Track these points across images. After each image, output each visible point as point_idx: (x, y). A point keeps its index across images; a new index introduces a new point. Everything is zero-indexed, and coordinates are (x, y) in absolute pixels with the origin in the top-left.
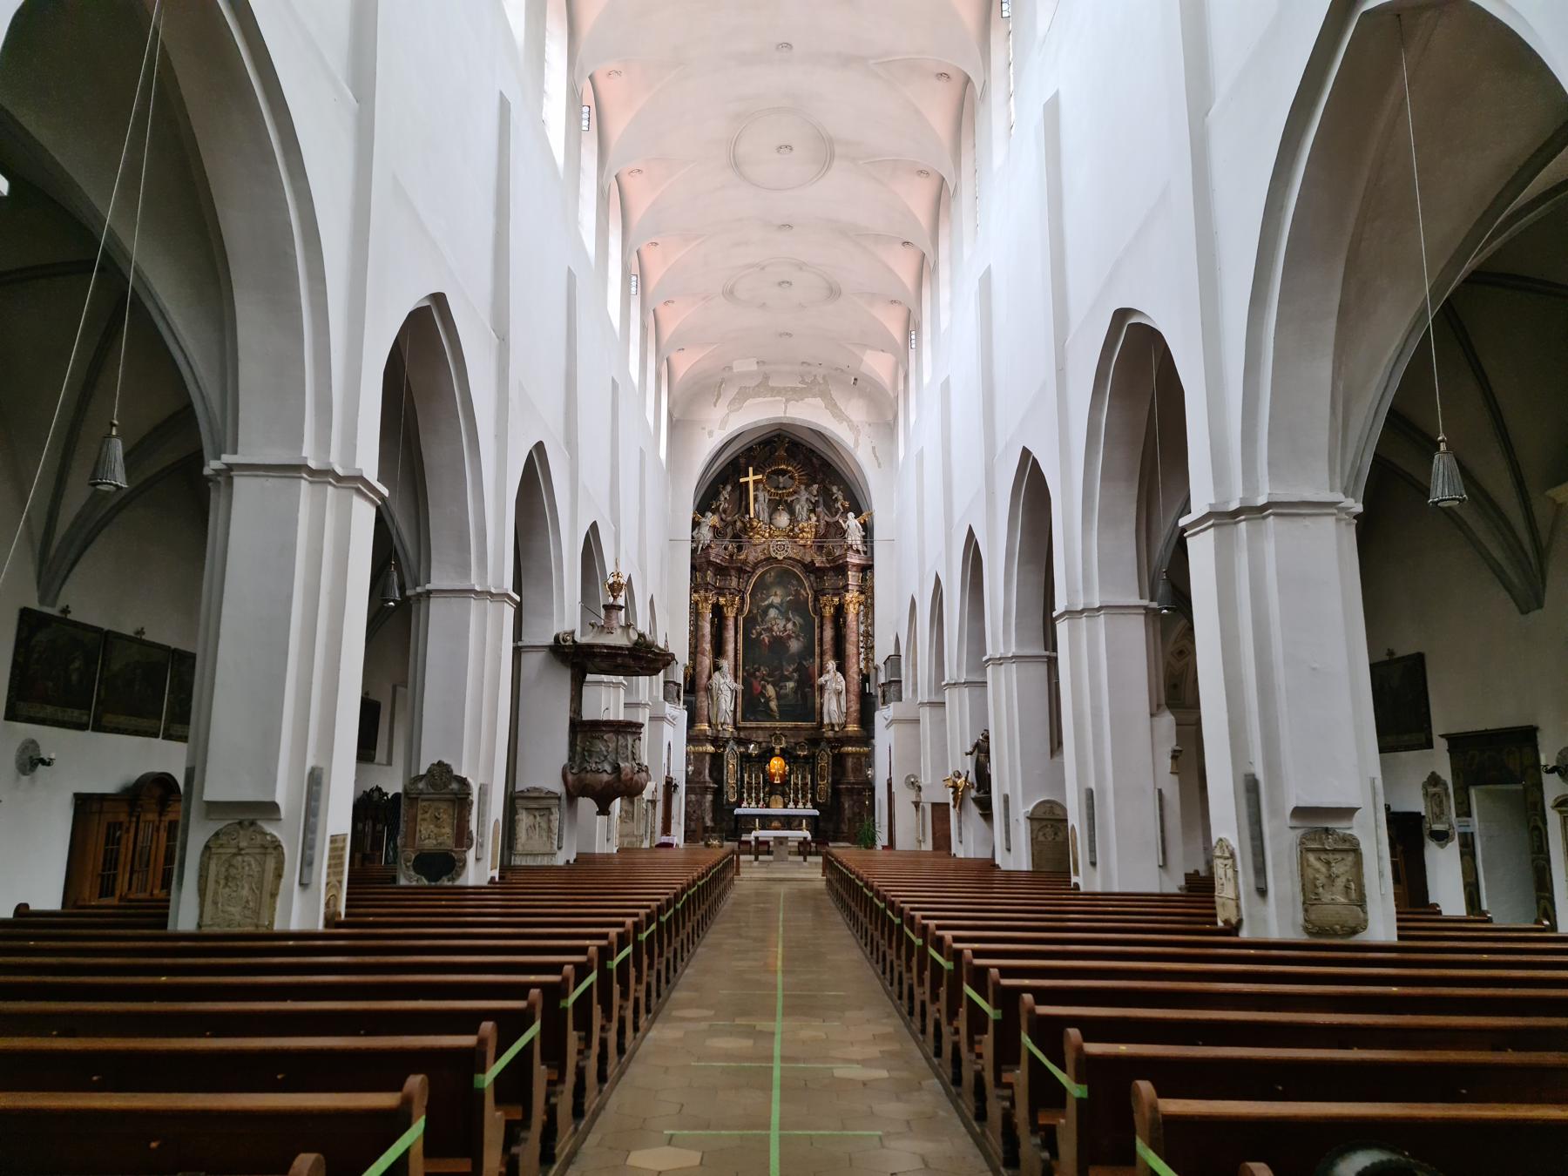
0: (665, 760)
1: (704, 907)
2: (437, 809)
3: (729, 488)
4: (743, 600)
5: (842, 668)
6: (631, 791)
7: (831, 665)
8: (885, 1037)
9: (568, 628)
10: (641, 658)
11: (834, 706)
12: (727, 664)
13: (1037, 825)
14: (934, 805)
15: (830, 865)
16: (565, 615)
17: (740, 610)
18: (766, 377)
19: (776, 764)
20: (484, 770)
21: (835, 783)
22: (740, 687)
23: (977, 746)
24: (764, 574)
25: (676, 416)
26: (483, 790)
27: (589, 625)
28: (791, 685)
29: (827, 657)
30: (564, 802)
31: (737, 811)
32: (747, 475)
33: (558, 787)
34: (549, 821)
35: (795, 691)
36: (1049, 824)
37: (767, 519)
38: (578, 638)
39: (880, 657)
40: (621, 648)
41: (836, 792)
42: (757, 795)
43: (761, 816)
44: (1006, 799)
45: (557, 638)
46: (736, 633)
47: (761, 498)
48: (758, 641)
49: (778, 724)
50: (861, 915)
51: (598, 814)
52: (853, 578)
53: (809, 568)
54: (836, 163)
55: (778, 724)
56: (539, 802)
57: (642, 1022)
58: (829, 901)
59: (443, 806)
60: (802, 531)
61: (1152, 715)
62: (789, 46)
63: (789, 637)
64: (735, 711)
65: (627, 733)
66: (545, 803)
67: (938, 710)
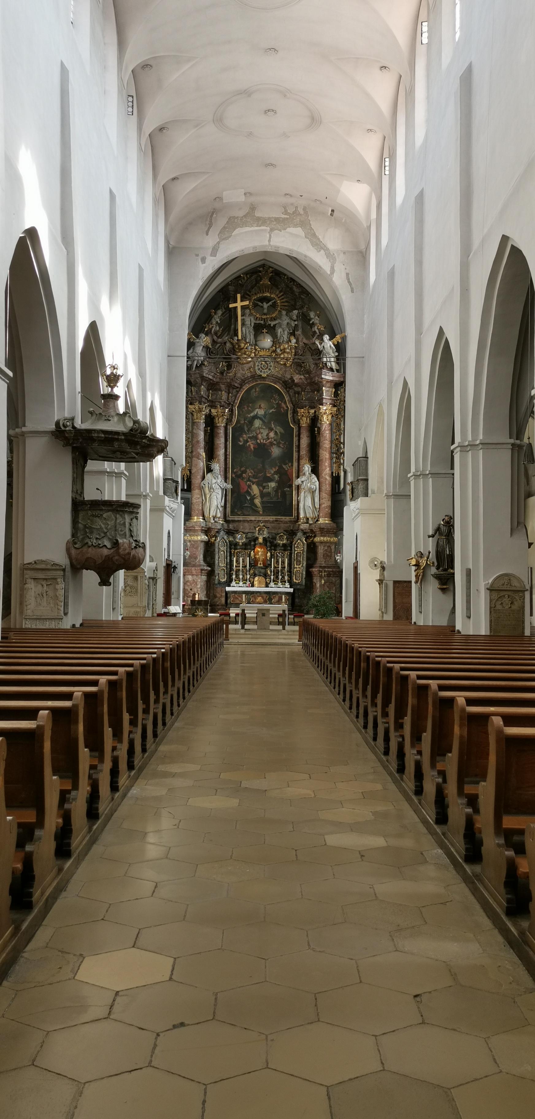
0: (165, 545)
1: (194, 668)
3: (220, 312)
4: (231, 411)
5: (315, 471)
6: (132, 563)
7: (307, 468)
9: (67, 415)
10: (136, 443)
11: (309, 502)
12: (217, 467)
13: (495, 595)
14: (395, 582)
16: (67, 403)
17: (229, 421)
18: (253, 208)
19: (260, 552)
21: (309, 566)
22: (230, 486)
23: (438, 530)
24: (252, 387)
25: (172, 243)
27: (88, 414)
28: (273, 485)
29: (302, 462)
31: (228, 589)
32: (235, 301)
33: (61, 558)
34: (56, 590)
35: (276, 490)
38: (79, 424)
40: (117, 433)
41: (309, 575)
42: (237, 576)
44: (468, 573)
45: (57, 424)
46: (226, 440)
47: (248, 322)
49: (261, 518)
52: (327, 393)
53: (288, 384)
56: (42, 571)
57: (123, 780)
60: (284, 351)
63: (271, 444)
64: (225, 507)
66: (50, 574)
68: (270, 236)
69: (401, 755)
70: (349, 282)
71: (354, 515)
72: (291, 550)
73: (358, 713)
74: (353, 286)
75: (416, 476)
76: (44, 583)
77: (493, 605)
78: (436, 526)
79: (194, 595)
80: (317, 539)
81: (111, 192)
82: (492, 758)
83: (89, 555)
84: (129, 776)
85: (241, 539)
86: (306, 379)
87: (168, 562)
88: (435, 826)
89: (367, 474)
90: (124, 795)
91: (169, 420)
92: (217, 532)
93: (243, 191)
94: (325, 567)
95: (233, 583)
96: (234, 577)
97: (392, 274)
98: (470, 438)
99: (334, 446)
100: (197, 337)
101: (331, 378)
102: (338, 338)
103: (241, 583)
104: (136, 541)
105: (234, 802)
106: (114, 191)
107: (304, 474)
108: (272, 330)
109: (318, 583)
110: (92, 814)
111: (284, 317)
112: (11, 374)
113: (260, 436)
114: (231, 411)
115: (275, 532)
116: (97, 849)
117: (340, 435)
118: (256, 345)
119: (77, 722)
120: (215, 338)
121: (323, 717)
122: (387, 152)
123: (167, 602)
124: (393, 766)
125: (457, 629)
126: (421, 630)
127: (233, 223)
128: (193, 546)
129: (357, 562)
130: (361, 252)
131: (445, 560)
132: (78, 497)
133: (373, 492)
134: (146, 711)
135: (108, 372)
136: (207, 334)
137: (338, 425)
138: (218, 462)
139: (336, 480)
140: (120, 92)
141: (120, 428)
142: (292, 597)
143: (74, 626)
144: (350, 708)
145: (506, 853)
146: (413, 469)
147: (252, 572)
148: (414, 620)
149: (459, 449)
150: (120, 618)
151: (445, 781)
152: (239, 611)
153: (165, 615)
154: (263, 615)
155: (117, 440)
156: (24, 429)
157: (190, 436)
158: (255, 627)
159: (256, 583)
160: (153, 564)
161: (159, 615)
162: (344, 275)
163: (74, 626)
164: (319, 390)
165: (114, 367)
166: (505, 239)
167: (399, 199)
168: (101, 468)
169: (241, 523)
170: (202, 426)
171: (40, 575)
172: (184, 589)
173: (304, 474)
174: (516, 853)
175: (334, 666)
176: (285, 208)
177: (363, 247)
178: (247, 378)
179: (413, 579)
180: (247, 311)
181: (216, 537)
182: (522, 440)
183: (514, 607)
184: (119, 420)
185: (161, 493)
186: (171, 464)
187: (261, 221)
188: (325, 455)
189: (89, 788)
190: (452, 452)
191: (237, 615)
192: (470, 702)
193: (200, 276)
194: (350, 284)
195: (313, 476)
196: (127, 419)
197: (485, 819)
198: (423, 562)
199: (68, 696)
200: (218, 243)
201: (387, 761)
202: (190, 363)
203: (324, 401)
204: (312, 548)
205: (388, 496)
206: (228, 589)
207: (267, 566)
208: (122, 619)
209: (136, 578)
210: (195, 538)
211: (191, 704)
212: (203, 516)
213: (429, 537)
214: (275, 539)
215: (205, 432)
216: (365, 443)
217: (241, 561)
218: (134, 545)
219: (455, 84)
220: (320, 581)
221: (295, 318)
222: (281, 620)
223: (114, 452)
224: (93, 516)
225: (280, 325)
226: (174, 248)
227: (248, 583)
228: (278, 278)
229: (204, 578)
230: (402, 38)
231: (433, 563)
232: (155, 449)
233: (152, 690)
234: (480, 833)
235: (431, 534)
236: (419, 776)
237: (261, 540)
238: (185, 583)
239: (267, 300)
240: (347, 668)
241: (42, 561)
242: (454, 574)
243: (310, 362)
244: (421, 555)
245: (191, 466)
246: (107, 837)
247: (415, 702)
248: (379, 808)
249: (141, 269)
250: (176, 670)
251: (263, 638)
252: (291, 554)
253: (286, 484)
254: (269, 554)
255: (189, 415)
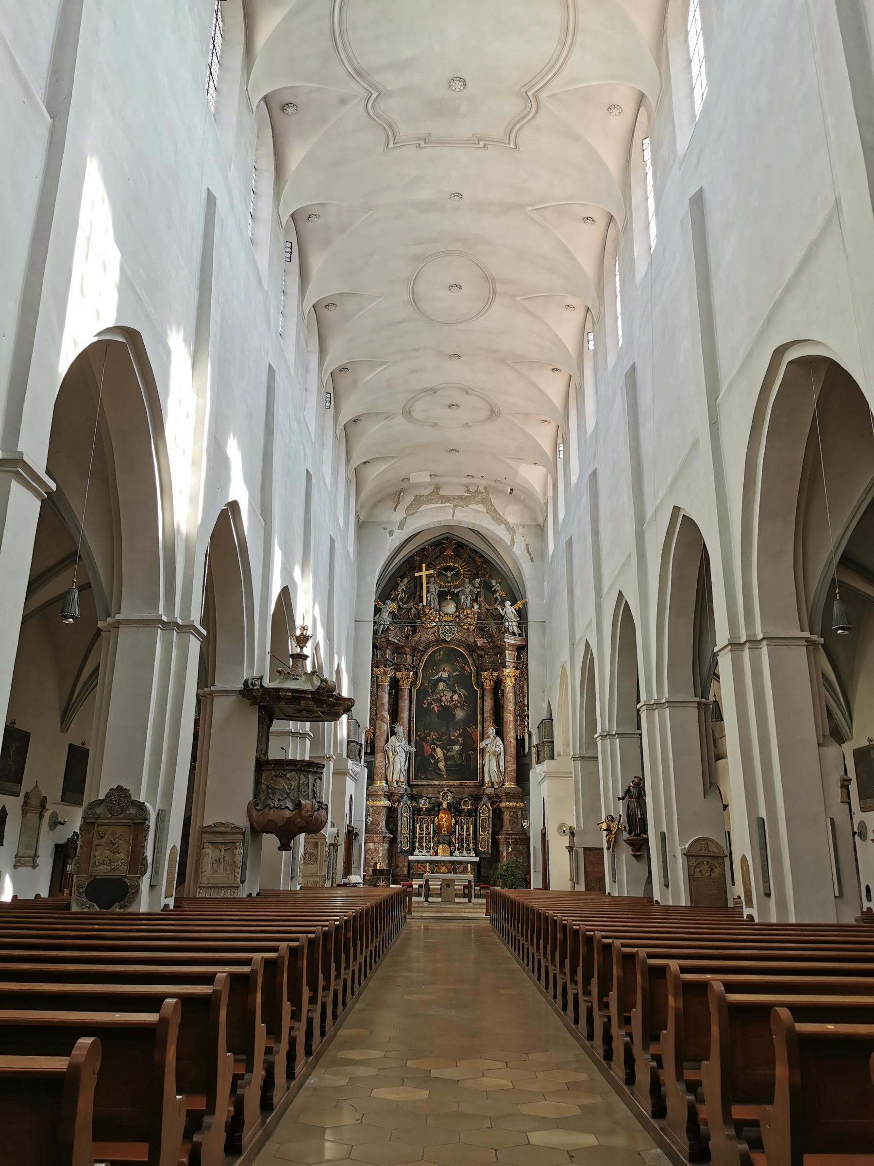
0: (347, 811)
1: (376, 943)
2: (113, 834)
3: (406, 581)
4: (416, 674)
5: (500, 734)
6: (313, 827)
7: (491, 731)
8: (572, 1087)
10: (324, 702)
11: (494, 766)
12: (400, 729)
13: (693, 861)
14: (586, 849)
15: (496, 902)
16: (258, 665)
17: (414, 683)
18: (438, 487)
19: (444, 818)
20: (164, 794)
21: (495, 834)
22: (413, 749)
23: (628, 792)
25: (362, 518)
26: (163, 816)
27: (278, 672)
28: (457, 748)
29: (486, 725)
30: (248, 837)
31: (411, 858)
33: (241, 820)
35: (460, 752)
36: (708, 862)
37: (437, 606)
38: (266, 683)
39: (533, 722)
40: (305, 692)
41: (495, 843)
43: (431, 862)
44: (663, 835)
45: (246, 682)
47: (432, 590)
48: (429, 710)
49: (444, 783)
50: (532, 950)
51: (281, 848)
52: (510, 656)
53: (472, 648)
54: (498, 300)
55: (444, 783)
56: (221, 834)
57: (300, 1067)
58: (495, 938)
59: (120, 830)
60: (467, 616)
61: (819, 745)
62: (460, 195)
63: (456, 706)
65: (308, 772)
67: (591, 763)
68: (454, 512)
69: (608, 1038)
70: (528, 552)
71: (540, 779)
72: (476, 816)
73: (555, 993)
74: (533, 555)
75: (603, 737)
76: (222, 848)
77: (692, 873)
78: (625, 788)
79: (376, 864)
80: (503, 804)
81: (307, 471)
82: (715, 1031)
83: (270, 818)
84: (307, 1062)
85: (425, 804)
86: (489, 643)
87: (351, 829)
88: (652, 1120)
89: (552, 737)
90: (301, 1085)
91: (354, 683)
92: (400, 797)
93: (429, 473)
94: (511, 834)
95: (417, 852)
96: (417, 844)
97: (570, 543)
98: (656, 697)
99: (518, 708)
100: (384, 604)
101: (513, 642)
102: (519, 604)
103: (424, 852)
104: (319, 802)
105: (424, 1094)
106: (311, 471)
107: (489, 737)
108: (455, 597)
109: (505, 852)
110: (266, 1105)
111: (467, 585)
112: (205, 632)
113: (444, 698)
114: (416, 674)
115: (460, 797)
116: (270, 1146)
117: (523, 698)
118: (440, 610)
119: (255, 991)
120: (401, 604)
121: (517, 997)
122: (561, 438)
123: (347, 872)
124: (599, 1052)
125: (655, 899)
126: (616, 901)
127: (418, 501)
128: (375, 812)
129: (545, 828)
130: (539, 526)
131: (637, 824)
132: (262, 757)
133: (559, 755)
134: (326, 988)
135: (298, 633)
136: (393, 601)
137: (522, 688)
138: (402, 724)
139: (520, 743)
140: (319, 390)
141: (308, 687)
142: (477, 866)
143: (250, 895)
144: (547, 988)
145: (739, 1146)
146: (599, 730)
147: (436, 839)
148: (608, 891)
149: (645, 707)
150: (298, 888)
151: (660, 1065)
152: (422, 882)
153: (345, 885)
154: (448, 886)
155: (304, 698)
156: (212, 688)
157: (374, 698)
158: (440, 900)
159: (440, 851)
160: (335, 830)
161: (338, 885)
162: (523, 547)
163: (250, 895)
164: (502, 653)
165: (304, 628)
166: (676, 509)
167: (574, 479)
168: (285, 729)
169: (425, 788)
170: (387, 689)
171: (219, 839)
172: (365, 858)
173: (489, 737)
174: (750, 1148)
175: (527, 940)
176: (467, 487)
177: (541, 521)
178: (432, 642)
179: (605, 846)
180: (432, 579)
181: (399, 802)
182: (707, 699)
183: (714, 875)
184: (306, 679)
185: (345, 756)
186: (355, 725)
187: (446, 499)
188: (509, 717)
189: (263, 1073)
190: (638, 710)
191: (421, 886)
192: (684, 970)
193: (388, 547)
194: (530, 554)
195: (498, 739)
196: (315, 677)
197: (711, 1110)
198: (614, 826)
199: (247, 962)
200: (405, 518)
201: (592, 1046)
202: (376, 627)
203: (507, 664)
204: (498, 814)
205: (574, 758)
206: (411, 858)
207: (451, 833)
208: (301, 888)
209: (316, 845)
210: (378, 803)
211: (373, 983)
212: (386, 780)
213: (619, 799)
214: (460, 804)
215: (390, 694)
216: (549, 704)
217: (425, 828)
218: (317, 806)
219: (620, 381)
220: (507, 849)
221: (477, 585)
222: (466, 891)
223: (301, 711)
224: (276, 776)
225: (463, 592)
226: (364, 522)
227: (432, 851)
228: (461, 549)
229: (386, 846)
230: (571, 346)
231: (625, 827)
232: (341, 708)
233: (329, 965)
234: (706, 1124)
235: (620, 796)
236: (630, 1061)
237: (445, 806)
238: (366, 852)
239: (451, 569)
240: (542, 941)
241: (222, 824)
242: (647, 839)
243: (493, 627)
244: (612, 819)
245: (375, 729)
246: (281, 1132)
247: (621, 973)
248: (586, 1101)
249: (332, 540)
250: (359, 942)
251: (449, 912)
252: (476, 820)
253: (471, 748)
254: (453, 820)
255: (375, 678)
